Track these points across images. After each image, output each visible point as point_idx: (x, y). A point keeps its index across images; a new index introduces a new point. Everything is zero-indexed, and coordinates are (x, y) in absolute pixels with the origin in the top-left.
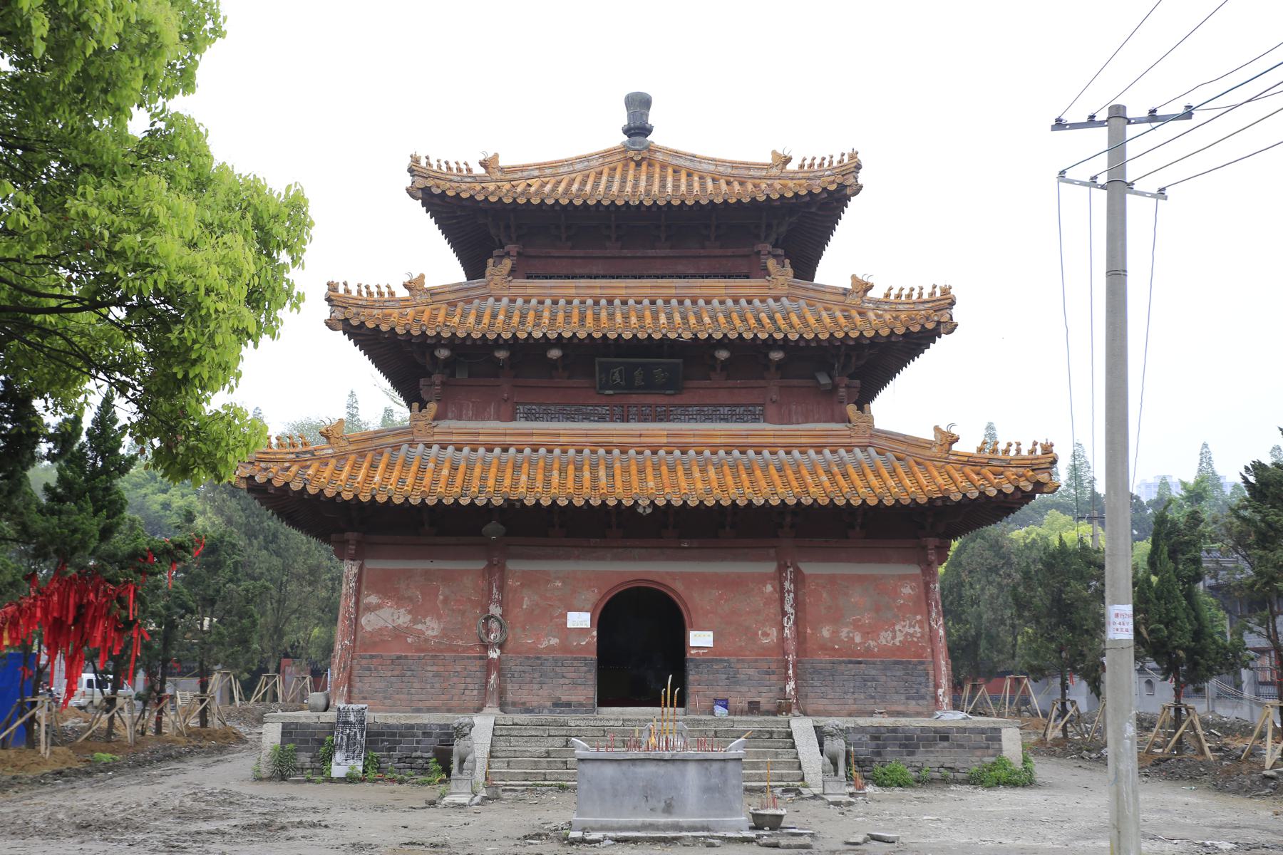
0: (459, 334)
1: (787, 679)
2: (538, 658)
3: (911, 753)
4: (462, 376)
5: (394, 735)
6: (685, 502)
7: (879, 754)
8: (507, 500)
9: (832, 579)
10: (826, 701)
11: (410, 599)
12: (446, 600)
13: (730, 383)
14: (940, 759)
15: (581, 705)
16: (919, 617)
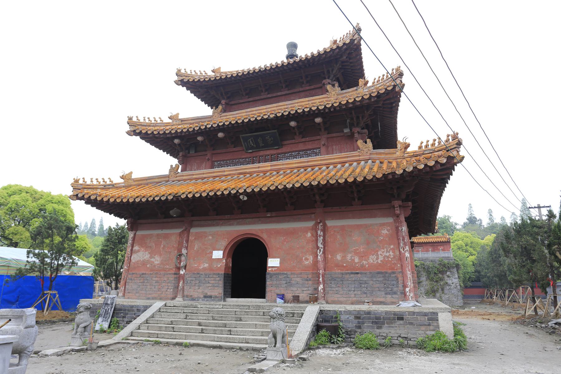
1: (319, 283)
2: (198, 274)
3: (380, 328)
4: (192, 152)
5: (125, 310)
7: (360, 327)
9: (343, 228)
10: (339, 296)
13: (303, 140)
14: (398, 331)
15: (216, 297)
16: (392, 247)
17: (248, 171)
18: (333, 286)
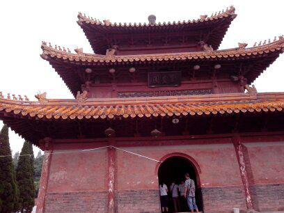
1: (246, 195)
4: (97, 83)
8: (115, 116)
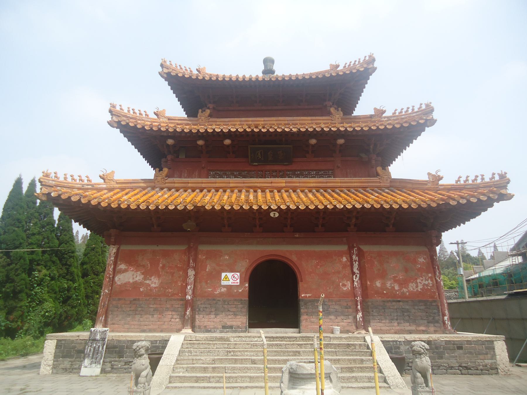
0: (178, 130)
1: (357, 311)
2: (214, 300)
6: (298, 207)
8: (196, 207)
11: (144, 266)
12: (163, 267)
15: (238, 327)
16: (430, 275)
17: (258, 185)
18: (374, 314)
